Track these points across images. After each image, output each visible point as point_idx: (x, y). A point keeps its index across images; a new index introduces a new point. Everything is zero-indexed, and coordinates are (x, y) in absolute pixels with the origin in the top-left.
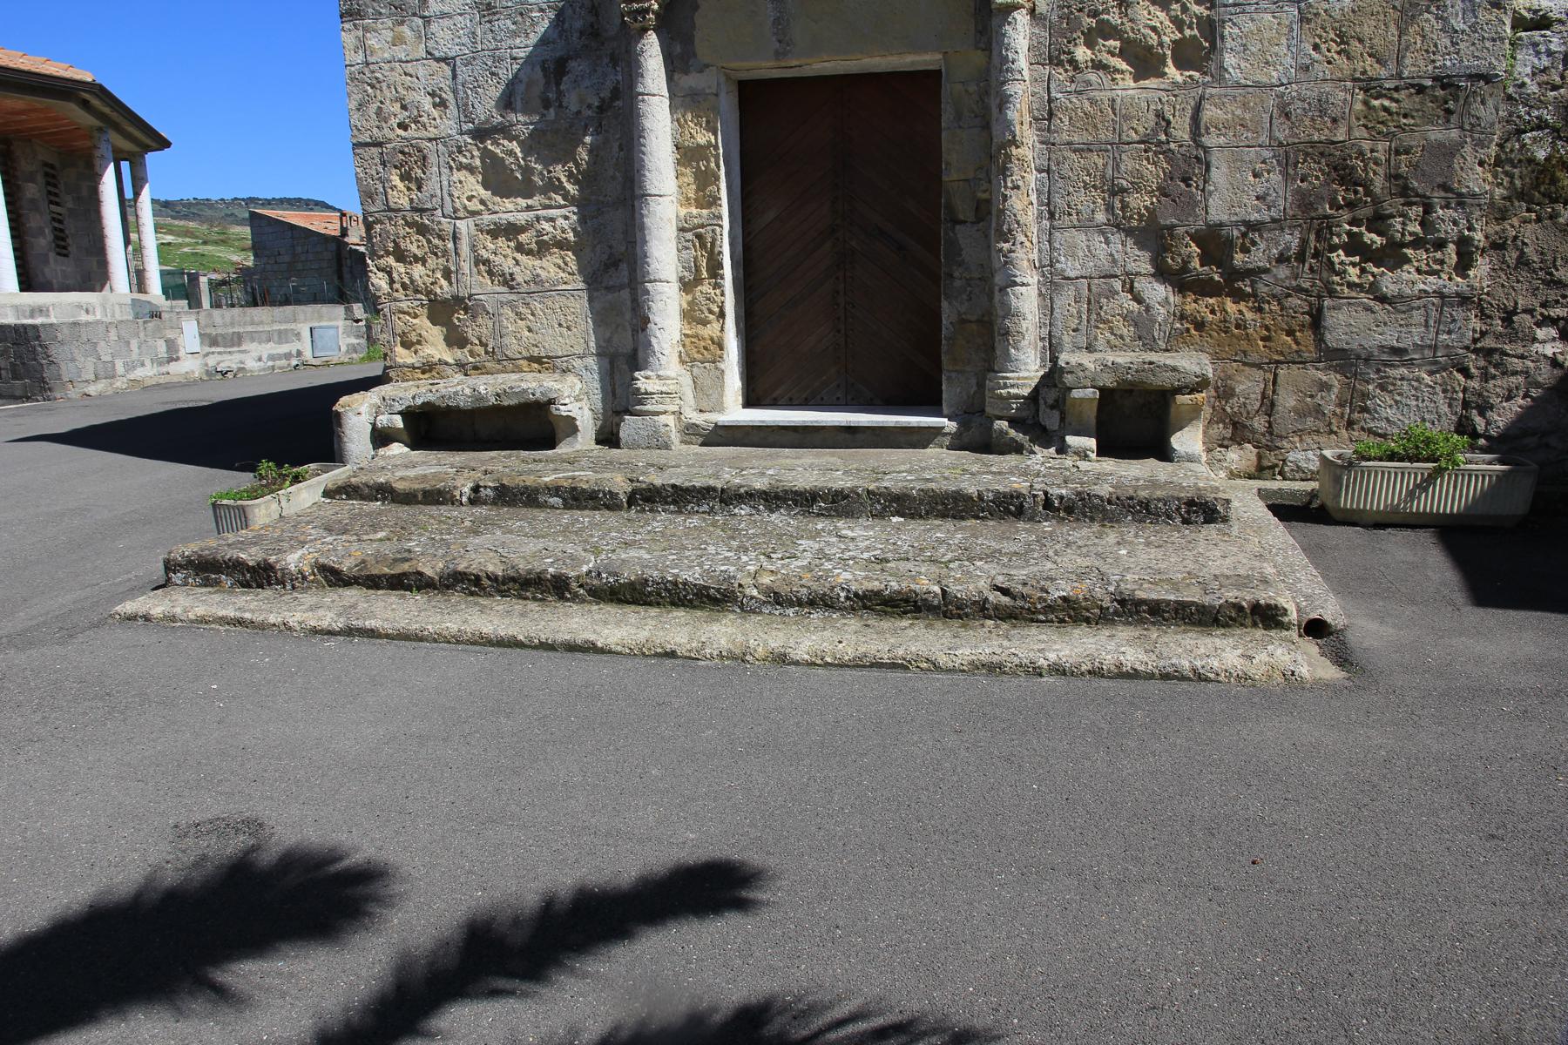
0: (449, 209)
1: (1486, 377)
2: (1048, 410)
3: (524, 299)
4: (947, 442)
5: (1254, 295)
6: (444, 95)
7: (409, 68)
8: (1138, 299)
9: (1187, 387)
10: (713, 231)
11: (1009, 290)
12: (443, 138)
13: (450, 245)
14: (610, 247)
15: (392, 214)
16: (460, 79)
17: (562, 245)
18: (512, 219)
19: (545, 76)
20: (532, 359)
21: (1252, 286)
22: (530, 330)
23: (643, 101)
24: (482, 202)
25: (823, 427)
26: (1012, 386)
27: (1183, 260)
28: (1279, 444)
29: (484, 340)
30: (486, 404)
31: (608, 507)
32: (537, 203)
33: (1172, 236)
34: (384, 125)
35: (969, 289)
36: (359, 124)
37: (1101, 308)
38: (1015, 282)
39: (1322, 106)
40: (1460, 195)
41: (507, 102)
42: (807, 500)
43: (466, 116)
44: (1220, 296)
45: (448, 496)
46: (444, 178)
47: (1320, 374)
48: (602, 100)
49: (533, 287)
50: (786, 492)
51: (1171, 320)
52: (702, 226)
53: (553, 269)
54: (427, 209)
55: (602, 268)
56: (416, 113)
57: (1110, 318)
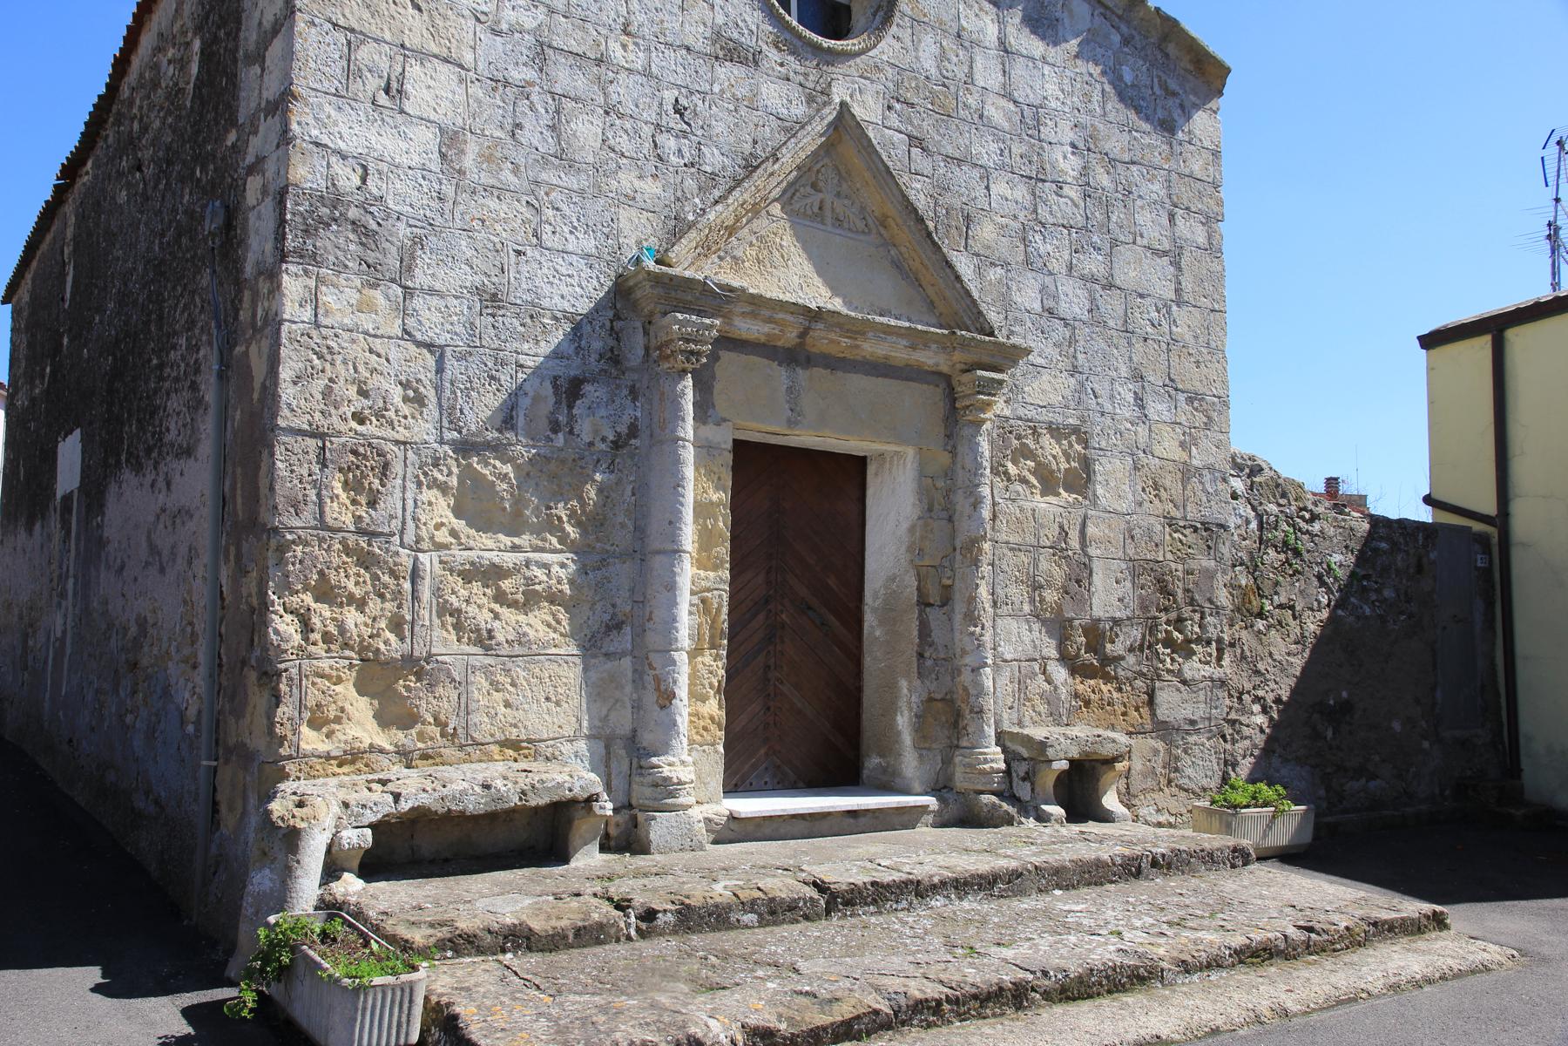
0: (409, 537)
1: (1234, 742)
3: (504, 664)
4: (930, 819)
5: (1116, 678)
6: (422, 389)
7: (378, 344)
10: (720, 596)
12: (416, 443)
13: (407, 586)
14: (614, 606)
15: (326, 534)
16: (448, 374)
17: (553, 598)
18: (496, 560)
19: (556, 394)
20: (506, 744)
22: (507, 705)
23: (684, 447)
24: (454, 533)
25: (829, 814)
26: (992, 761)
29: (442, 717)
30: (507, 806)
31: (807, 918)
32: (527, 543)
33: (1071, 626)
34: (333, 411)
36: (295, 403)
39: (1149, 532)
40: (1217, 607)
41: (507, 418)
43: (451, 422)
45: (613, 931)
46: (409, 495)
47: (1153, 742)
48: (619, 435)
49: (517, 650)
50: (972, 876)
52: (708, 590)
53: (542, 628)
54: (382, 534)
55: (603, 630)
56: (381, 404)
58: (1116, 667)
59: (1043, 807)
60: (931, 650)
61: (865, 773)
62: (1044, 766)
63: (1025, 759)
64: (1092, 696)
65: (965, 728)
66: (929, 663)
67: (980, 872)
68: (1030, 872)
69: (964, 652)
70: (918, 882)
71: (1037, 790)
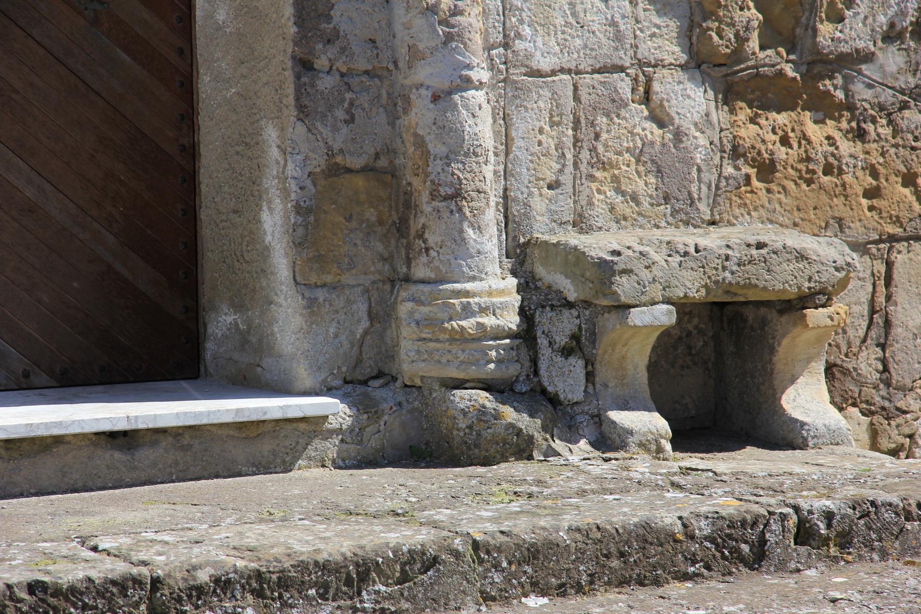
2: (559, 359)
4: (331, 447)
5: (850, 107)
8: (660, 119)
9: (822, 292)
11: (456, 97)
21: (846, 90)
25: (58, 440)
26: (483, 310)
27: (737, 35)
28: (901, 404)
35: (348, 96)
37: (597, 136)
38: (468, 80)
42: (349, 582)
44: (793, 109)
50: (302, 566)
51: (717, 160)
57: (614, 157)
58: (848, 80)
59: (615, 415)
60: (332, 51)
61: (210, 348)
62: (611, 319)
63: (570, 305)
64: (781, 152)
65: (420, 236)
66: (326, 83)
67: (322, 558)
68: (457, 554)
69: (415, 55)
70: (156, 582)
71: (603, 373)
